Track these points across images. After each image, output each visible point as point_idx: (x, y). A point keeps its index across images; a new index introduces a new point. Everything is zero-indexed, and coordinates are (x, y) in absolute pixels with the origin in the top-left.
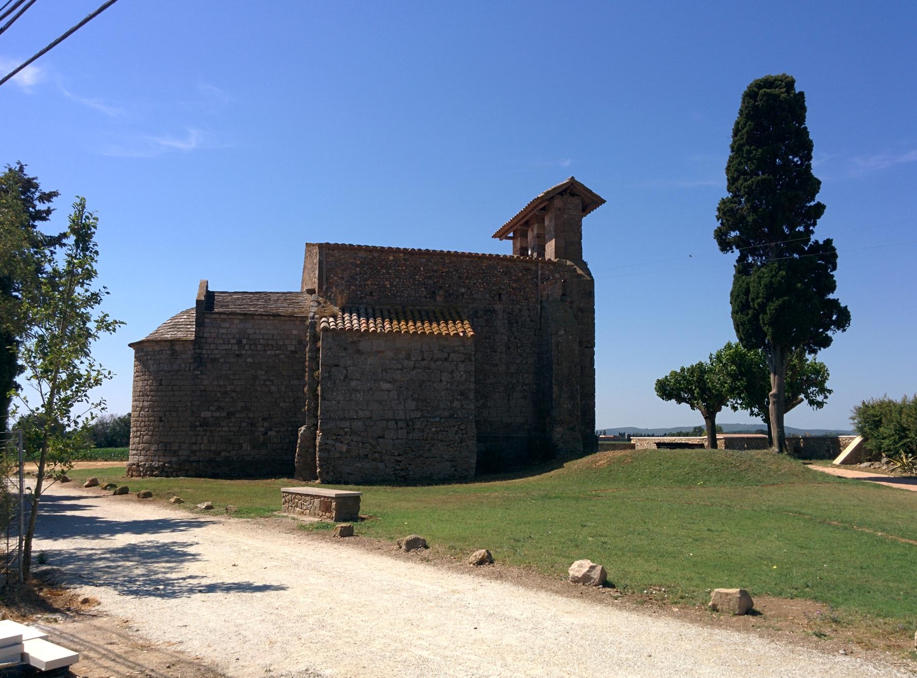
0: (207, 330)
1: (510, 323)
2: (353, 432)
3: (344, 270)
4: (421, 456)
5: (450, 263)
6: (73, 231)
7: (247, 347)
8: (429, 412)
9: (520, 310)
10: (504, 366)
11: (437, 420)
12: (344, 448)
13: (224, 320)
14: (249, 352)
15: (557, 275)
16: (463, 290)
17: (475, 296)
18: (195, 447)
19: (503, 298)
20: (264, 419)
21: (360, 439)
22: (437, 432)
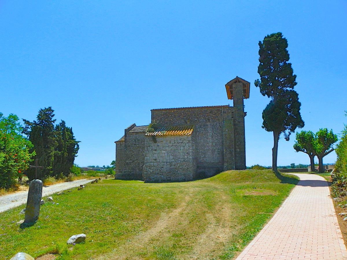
0: (127, 138)
1: (213, 129)
2: (154, 166)
3: (159, 117)
4: (174, 174)
5: (192, 111)
6: (293, 91)
7: (137, 142)
8: (177, 160)
9: (216, 124)
10: (211, 143)
11: (180, 162)
12: (152, 171)
13: (131, 135)
14: (138, 143)
15: (230, 111)
16: (196, 119)
17: (200, 121)
18: (125, 171)
19: (210, 120)
20: (142, 162)
21: (156, 168)
22: (179, 166)
